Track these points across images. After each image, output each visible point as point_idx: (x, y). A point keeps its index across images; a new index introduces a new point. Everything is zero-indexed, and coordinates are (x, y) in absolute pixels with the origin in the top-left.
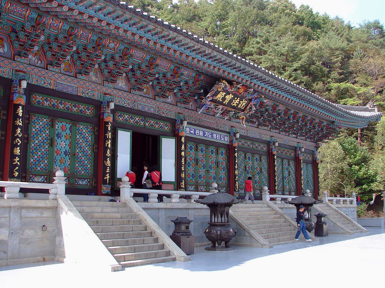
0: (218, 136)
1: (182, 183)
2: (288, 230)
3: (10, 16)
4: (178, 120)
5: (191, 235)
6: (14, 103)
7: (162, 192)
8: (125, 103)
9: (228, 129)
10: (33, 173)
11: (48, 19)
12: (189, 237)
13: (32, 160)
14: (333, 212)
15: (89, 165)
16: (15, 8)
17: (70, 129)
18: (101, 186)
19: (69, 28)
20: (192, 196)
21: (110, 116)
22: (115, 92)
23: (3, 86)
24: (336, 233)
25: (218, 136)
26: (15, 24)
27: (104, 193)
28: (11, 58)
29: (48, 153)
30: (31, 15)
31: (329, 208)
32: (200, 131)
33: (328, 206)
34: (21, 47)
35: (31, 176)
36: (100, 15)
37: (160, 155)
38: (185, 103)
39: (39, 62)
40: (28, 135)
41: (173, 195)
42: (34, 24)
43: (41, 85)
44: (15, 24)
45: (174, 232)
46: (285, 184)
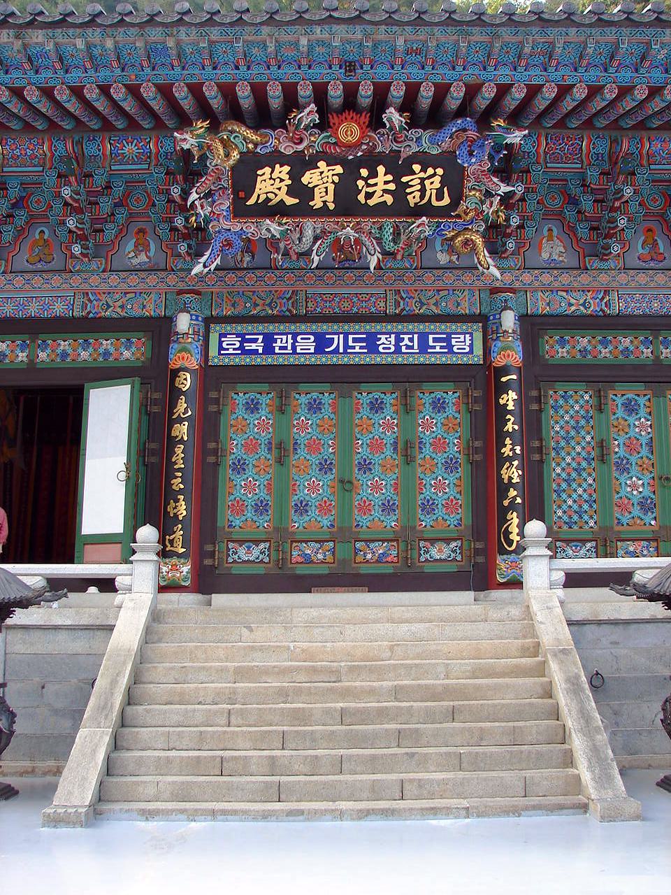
0: (406, 341)
1: (172, 537)
2: (537, 741)
3: (654, 170)
4: (196, 316)
6: (494, 367)
8: (570, 305)
9: (471, 304)
11: (534, 141)
16: (13, 147)
17: (334, 405)
19: (611, 145)
21: (510, 348)
22: (527, 277)
23: (151, 333)
25: (411, 340)
26: (564, 183)
27: (502, 581)
28: (112, 269)
30: (593, 148)
32: (351, 337)
34: (595, 232)
36: (652, 75)
37: (82, 448)
38: (603, 253)
39: (247, 258)
40: (541, 440)
41: (117, 577)
42: (607, 167)
43: (560, 311)
44: (564, 183)
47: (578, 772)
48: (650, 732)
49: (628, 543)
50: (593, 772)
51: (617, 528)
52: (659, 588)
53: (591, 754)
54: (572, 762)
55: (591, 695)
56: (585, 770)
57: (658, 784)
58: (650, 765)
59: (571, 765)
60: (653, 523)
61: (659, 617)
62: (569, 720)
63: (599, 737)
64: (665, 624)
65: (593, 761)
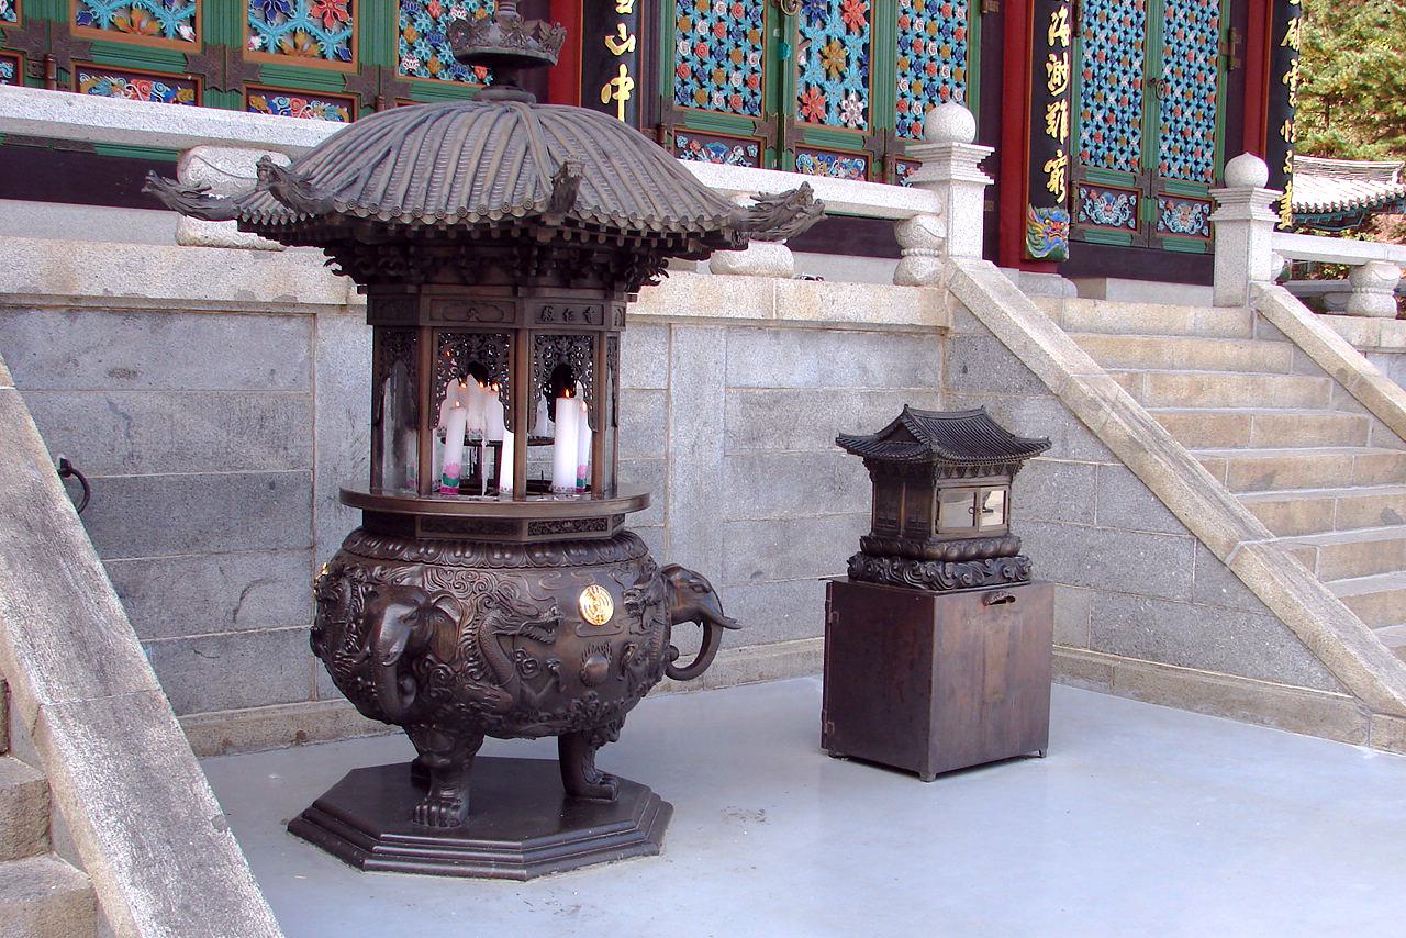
5: (1022, 577)
7: (29, 113)
10: (691, 126)
12: (1012, 599)
13: (684, 48)
14: (1310, 403)
15: (757, 55)
18: (1023, 214)
20: (185, 151)
24: (1225, 703)
27: (1038, 255)
29: (964, 49)
31: (1275, 352)
33: (1264, 325)
35: (900, 172)
45: (871, 548)
46: (815, 73)
47: (80, 878)
48: (225, 644)
49: (115, 81)
50: (154, 884)
51: (80, 32)
52: (354, 194)
53: (136, 807)
54: (48, 832)
55: (98, 565)
56: (124, 879)
57: (295, 828)
58: (227, 743)
59: (43, 843)
60: (186, 31)
61: (262, 298)
62: (34, 677)
63: (155, 733)
64: (277, 321)
65: (152, 833)
